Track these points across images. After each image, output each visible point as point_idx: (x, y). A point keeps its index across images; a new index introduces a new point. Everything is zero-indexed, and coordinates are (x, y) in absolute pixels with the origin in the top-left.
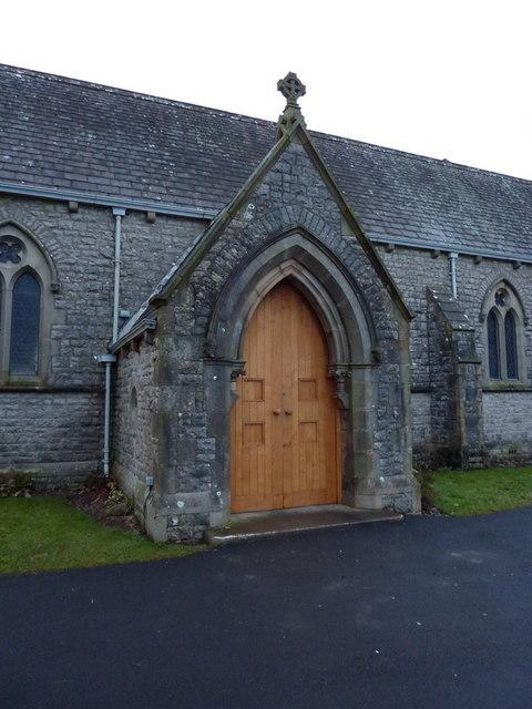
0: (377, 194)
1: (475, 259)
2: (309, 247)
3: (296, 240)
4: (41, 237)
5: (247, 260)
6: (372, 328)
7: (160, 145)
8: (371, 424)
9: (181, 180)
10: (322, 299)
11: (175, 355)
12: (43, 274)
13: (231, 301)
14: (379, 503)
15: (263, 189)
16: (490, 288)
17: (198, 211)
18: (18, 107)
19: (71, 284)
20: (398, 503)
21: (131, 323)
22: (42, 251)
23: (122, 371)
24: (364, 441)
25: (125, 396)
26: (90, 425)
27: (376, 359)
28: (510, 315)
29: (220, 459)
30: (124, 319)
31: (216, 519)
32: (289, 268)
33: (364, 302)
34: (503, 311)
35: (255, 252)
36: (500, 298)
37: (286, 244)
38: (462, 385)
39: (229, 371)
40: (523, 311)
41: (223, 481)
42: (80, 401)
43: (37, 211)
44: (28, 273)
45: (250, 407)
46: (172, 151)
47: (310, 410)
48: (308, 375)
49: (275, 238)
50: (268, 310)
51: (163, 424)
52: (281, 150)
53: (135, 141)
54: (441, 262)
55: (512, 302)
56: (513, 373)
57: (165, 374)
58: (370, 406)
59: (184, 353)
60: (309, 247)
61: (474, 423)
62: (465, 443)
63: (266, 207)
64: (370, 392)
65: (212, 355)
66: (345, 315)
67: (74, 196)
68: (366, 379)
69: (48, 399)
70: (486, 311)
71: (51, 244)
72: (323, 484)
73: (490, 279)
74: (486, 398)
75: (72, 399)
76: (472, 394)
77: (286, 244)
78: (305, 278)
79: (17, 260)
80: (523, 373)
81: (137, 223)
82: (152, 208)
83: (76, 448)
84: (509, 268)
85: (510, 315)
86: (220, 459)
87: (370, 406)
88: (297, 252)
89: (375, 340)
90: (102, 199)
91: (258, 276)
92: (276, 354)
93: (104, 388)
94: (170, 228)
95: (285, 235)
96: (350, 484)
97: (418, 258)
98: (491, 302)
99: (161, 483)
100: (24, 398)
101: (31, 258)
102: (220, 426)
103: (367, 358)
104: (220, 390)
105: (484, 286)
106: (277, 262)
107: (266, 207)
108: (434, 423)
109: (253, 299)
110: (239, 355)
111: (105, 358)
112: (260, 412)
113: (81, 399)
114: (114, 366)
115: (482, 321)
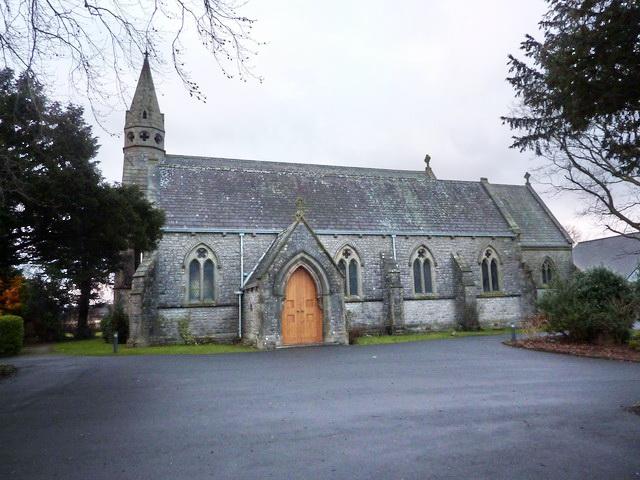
0: (359, 207)
1: (406, 237)
2: (306, 257)
3: (302, 254)
4: (212, 246)
5: (285, 263)
6: (329, 282)
7: (256, 198)
8: (330, 314)
9: (266, 215)
10: (312, 273)
11: (264, 294)
12: (214, 261)
13: (281, 277)
14: (332, 340)
15: (290, 239)
16: (415, 250)
17: (273, 230)
18: (197, 188)
19: (225, 265)
20: (340, 340)
21: (248, 278)
22: (214, 253)
23: (246, 297)
24: (328, 320)
25: (247, 307)
26: (234, 318)
27: (331, 293)
28: (427, 262)
29: (279, 326)
30: (246, 277)
31: (278, 343)
32: (300, 264)
33: (326, 273)
34: (422, 260)
35: (288, 260)
36: (421, 254)
37: (299, 256)
38: (393, 297)
39: (281, 298)
40: (434, 258)
41: (280, 332)
42: (230, 310)
43: (211, 237)
44: (209, 262)
45: (289, 309)
46: (262, 200)
47: (310, 310)
48: (309, 298)
49: (294, 255)
50: (294, 277)
51: (261, 315)
52: (296, 225)
53: (246, 197)
54: (387, 240)
55: (428, 255)
56: (429, 288)
57: (261, 300)
58: (329, 308)
59: (267, 294)
60: (306, 257)
61: (399, 314)
62: (394, 324)
63: (291, 245)
64: (329, 303)
65: (275, 294)
66: (320, 277)
67: (225, 230)
68: (328, 299)
69: (218, 309)
70: (413, 262)
71: (217, 250)
72: (314, 335)
73: (415, 246)
74: (406, 303)
75: (227, 309)
76: (397, 301)
77: (299, 256)
78: (306, 266)
79: (204, 256)
80: (435, 290)
81: (249, 238)
82: (254, 231)
83: (230, 328)
84: (426, 239)
85: (427, 262)
86: (279, 326)
87: (329, 308)
88: (302, 259)
89: (331, 285)
90: (236, 230)
91: (290, 267)
92: (297, 291)
93: (238, 304)
94: (262, 238)
95: (299, 253)
96: (324, 335)
97: (375, 239)
98: (416, 256)
99: (261, 333)
100: (208, 309)
101: (210, 256)
102: (279, 315)
103: (328, 292)
104: (278, 305)
105: (412, 249)
106: (296, 262)
107: (291, 245)
108: (384, 315)
109: (288, 275)
110: (284, 292)
111: (239, 292)
112: (292, 311)
113: (230, 309)
114: (242, 295)
115: (410, 266)
